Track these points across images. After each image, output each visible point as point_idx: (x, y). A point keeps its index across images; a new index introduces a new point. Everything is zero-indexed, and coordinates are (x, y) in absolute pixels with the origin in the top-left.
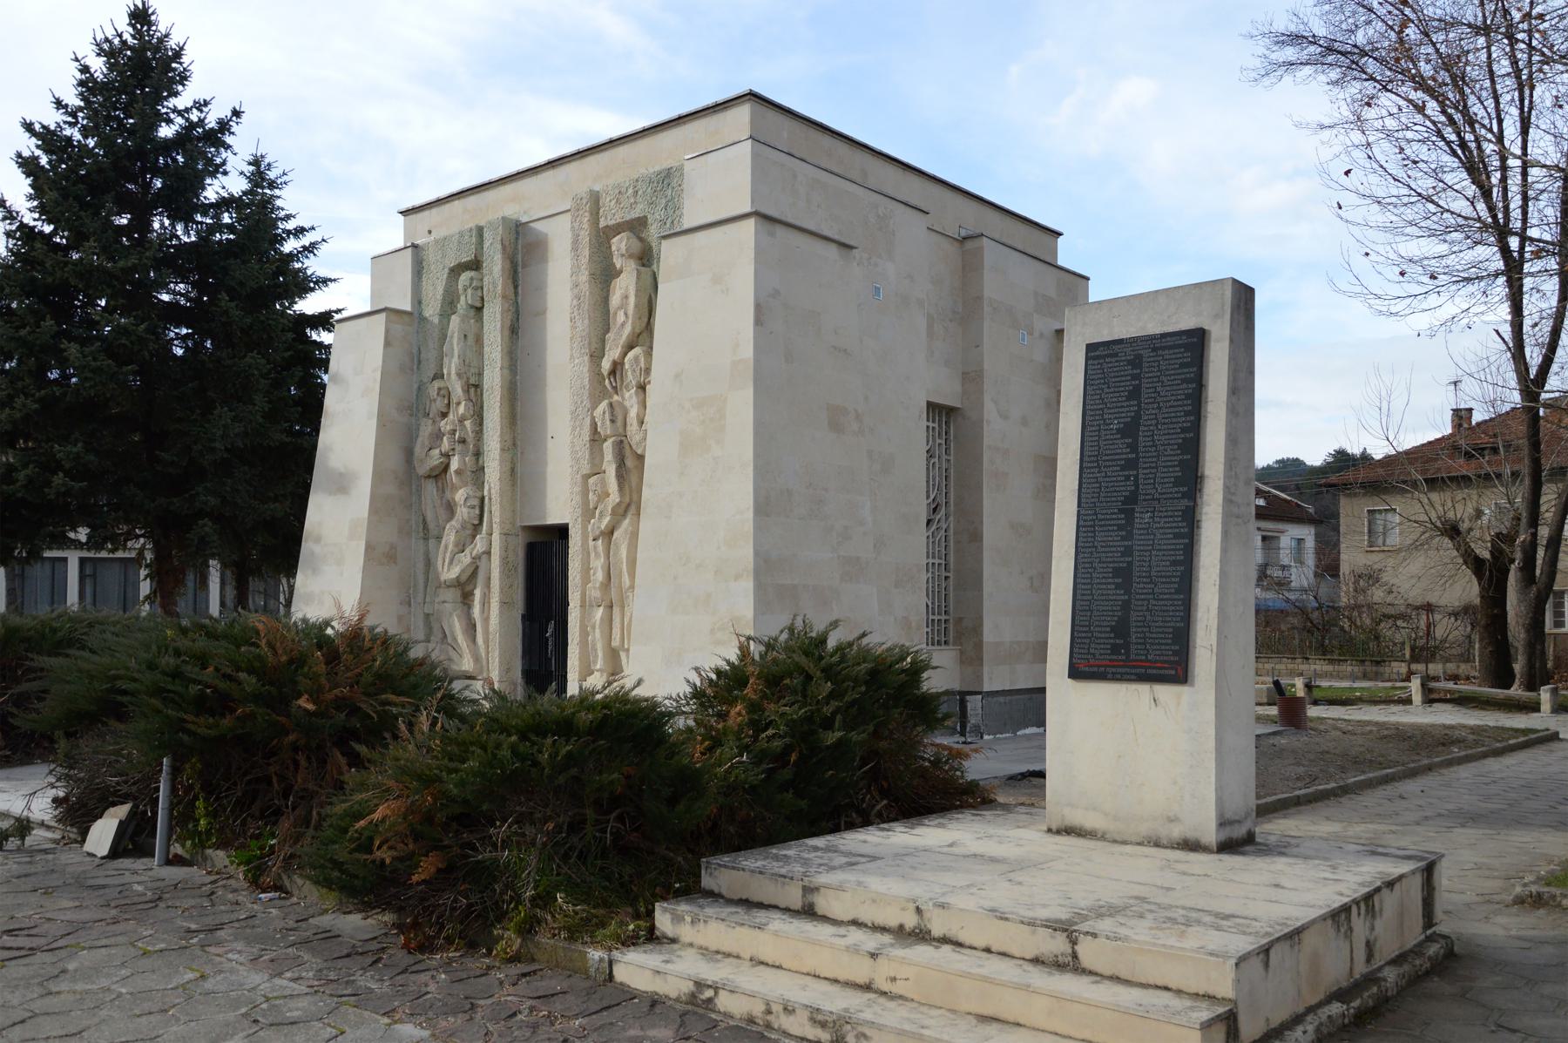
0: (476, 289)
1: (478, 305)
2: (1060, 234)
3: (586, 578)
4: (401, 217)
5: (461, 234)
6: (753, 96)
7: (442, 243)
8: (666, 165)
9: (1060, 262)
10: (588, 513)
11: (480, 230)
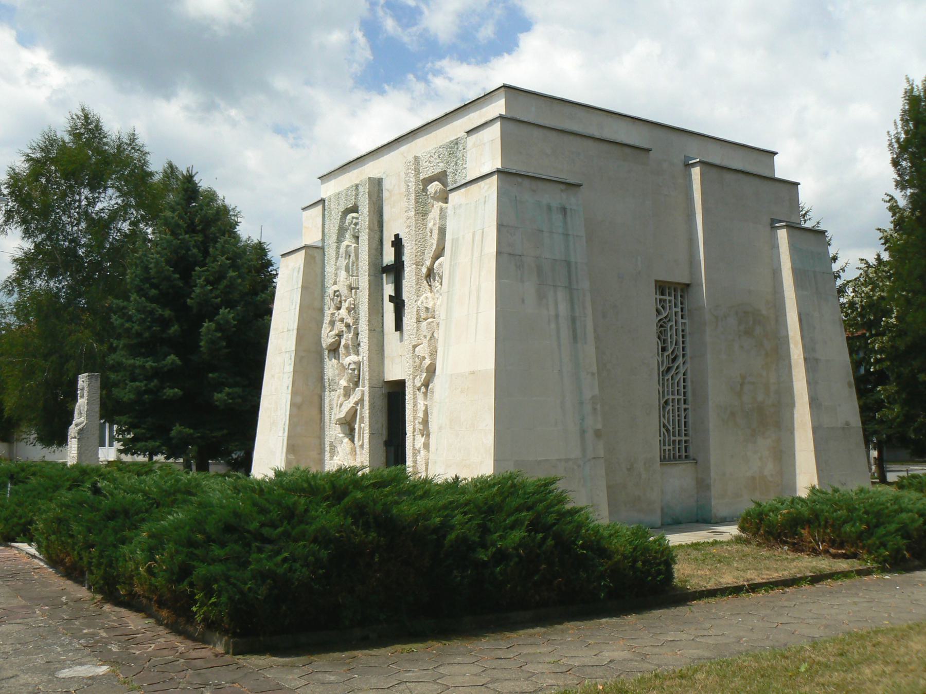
0: (356, 224)
2: (775, 153)
5: (348, 189)
6: (505, 87)
10: (417, 368)
11: (357, 186)
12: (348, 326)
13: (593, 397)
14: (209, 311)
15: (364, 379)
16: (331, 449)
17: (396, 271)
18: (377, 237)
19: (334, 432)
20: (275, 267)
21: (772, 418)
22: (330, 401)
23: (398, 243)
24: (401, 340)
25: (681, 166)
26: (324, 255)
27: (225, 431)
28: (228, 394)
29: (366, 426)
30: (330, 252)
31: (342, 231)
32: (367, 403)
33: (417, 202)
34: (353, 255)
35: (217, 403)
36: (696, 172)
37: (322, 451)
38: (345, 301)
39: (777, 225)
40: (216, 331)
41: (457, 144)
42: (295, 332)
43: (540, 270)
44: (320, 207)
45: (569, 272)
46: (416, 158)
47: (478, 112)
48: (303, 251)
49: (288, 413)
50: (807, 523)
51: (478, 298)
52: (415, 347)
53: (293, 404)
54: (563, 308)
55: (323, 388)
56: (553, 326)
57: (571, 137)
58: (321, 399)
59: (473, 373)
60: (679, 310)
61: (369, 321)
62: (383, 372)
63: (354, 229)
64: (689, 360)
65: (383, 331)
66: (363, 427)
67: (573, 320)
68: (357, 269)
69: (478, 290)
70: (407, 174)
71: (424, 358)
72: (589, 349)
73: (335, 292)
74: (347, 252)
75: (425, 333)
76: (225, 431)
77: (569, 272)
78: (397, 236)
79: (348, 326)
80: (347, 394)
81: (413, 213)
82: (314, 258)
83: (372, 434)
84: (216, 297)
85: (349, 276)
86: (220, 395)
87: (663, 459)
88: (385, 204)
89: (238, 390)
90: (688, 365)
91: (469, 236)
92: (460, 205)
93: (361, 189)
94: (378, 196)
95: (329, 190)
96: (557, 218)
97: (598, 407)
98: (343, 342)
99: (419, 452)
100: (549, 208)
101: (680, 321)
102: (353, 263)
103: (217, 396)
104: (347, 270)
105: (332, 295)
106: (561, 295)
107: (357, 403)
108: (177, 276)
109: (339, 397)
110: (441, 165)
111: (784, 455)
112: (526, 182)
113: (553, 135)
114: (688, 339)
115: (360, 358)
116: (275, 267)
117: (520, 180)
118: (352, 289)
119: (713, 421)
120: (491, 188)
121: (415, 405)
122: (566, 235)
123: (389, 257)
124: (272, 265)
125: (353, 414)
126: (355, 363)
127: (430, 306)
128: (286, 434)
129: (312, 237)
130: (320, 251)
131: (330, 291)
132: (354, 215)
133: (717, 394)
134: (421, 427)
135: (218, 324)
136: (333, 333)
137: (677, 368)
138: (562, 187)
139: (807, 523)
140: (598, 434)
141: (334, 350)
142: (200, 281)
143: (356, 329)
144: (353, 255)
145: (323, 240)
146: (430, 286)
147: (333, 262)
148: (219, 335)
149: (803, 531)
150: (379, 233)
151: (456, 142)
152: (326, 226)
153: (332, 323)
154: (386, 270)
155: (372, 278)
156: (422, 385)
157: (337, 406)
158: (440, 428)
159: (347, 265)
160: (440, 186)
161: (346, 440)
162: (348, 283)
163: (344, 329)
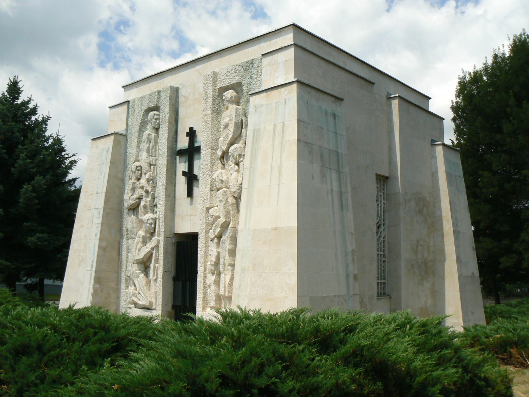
0: (156, 119)
1: (157, 127)
2: (430, 98)
3: (206, 262)
4: (123, 89)
5: (150, 94)
6: (294, 25)
7: (142, 99)
8: (250, 58)
9: (431, 110)
10: (209, 226)
11: (159, 92)
12: (147, 192)
13: (353, 251)
14: (26, 177)
15: (159, 231)
16: (126, 281)
17: (192, 152)
18: (174, 129)
19: (131, 269)
20: (67, 152)
21: (429, 269)
22: (128, 247)
23: (192, 134)
24: (191, 203)
25: (385, 98)
26: (127, 140)
27: (33, 265)
28: (38, 238)
29: (160, 266)
30: (133, 139)
31: (143, 125)
32: (161, 249)
33: (213, 104)
34: (153, 141)
35: (30, 244)
36: (395, 103)
37: (119, 282)
38: (145, 174)
39: (436, 143)
40: (31, 192)
41: (252, 63)
42: (104, 195)
43: (322, 156)
44: (125, 107)
45: (338, 159)
46: (214, 73)
47: (268, 43)
48: (112, 137)
49: (96, 253)
50: (515, 344)
51: (280, 173)
52: (208, 209)
53: (100, 247)
54: (335, 184)
55: (122, 236)
56: (330, 197)
57: (333, 67)
58: (120, 245)
59: (276, 229)
60: (382, 194)
61: (166, 189)
62: (174, 227)
63: (155, 122)
64: (386, 228)
65: (175, 197)
66: (159, 268)
67: (341, 194)
68: (155, 152)
69: (280, 167)
70: (205, 84)
71: (218, 217)
72: (350, 215)
73: (137, 167)
74: (148, 138)
75: (220, 199)
76: (33, 265)
77: (338, 159)
78: (191, 129)
79: (147, 192)
80: (145, 242)
81: (210, 112)
82: (120, 142)
83: (164, 272)
84: (33, 168)
85: (151, 156)
86: (32, 239)
87: (378, 295)
88: (180, 106)
89: (45, 235)
90: (386, 232)
91: (270, 128)
92: (261, 106)
93: (163, 94)
94: (176, 100)
95: (133, 94)
96: (331, 120)
97: (355, 258)
98: (142, 203)
99: (210, 286)
100: (326, 113)
101: (383, 201)
102: (153, 147)
103: (30, 239)
104: (148, 151)
105: (134, 170)
106: (334, 175)
107: (153, 249)
108: (5, 151)
109: (138, 243)
110: (237, 78)
111: (438, 294)
112: (313, 92)
113: (323, 63)
114: (386, 214)
115: (157, 215)
116: (67, 152)
117: (309, 90)
118: (151, 165)
119: (403, 271)
120: (291, 94)
121: (206, 252)
122: (336, 133)
123: (183, 143)
124: (64, 151)
125: (149, 256)
126: (152, 219)
127: (224, 179)
128: (94, 269)
129: (121, 128)
130: (123, 137)
131: (133, 166)
132: (156, 112)
133: (405, 253)
134: (213, 268)
135: (34, 187)
136: (135, 196)
137: (381, 233)
138: (333, 99)
139: (515, 344)
140: (355, 277)
141: (134, 209)
142: (23, 155)
143: (153, 194)
144: (153, 141)
145: (127, 130)
146: (223, 165)
147: (134, 145)
148: (34, 195)
149: (512, 350)
150: (175, 126)
151: (252, 62)
152: (130, 120)
153: (133, 189)
154: (181, 153)
155: (169, 158)
156: (216, 237)
157: (135, 250)
158: (243, 270)
159: (148, 147)
160: (235, 93)
161: (142, 275)
162: (148, 161)
163: (144, 194)
